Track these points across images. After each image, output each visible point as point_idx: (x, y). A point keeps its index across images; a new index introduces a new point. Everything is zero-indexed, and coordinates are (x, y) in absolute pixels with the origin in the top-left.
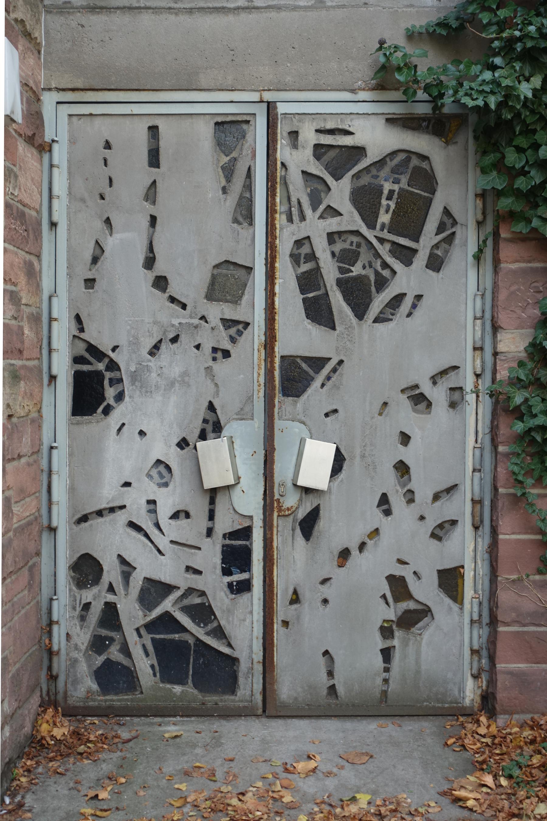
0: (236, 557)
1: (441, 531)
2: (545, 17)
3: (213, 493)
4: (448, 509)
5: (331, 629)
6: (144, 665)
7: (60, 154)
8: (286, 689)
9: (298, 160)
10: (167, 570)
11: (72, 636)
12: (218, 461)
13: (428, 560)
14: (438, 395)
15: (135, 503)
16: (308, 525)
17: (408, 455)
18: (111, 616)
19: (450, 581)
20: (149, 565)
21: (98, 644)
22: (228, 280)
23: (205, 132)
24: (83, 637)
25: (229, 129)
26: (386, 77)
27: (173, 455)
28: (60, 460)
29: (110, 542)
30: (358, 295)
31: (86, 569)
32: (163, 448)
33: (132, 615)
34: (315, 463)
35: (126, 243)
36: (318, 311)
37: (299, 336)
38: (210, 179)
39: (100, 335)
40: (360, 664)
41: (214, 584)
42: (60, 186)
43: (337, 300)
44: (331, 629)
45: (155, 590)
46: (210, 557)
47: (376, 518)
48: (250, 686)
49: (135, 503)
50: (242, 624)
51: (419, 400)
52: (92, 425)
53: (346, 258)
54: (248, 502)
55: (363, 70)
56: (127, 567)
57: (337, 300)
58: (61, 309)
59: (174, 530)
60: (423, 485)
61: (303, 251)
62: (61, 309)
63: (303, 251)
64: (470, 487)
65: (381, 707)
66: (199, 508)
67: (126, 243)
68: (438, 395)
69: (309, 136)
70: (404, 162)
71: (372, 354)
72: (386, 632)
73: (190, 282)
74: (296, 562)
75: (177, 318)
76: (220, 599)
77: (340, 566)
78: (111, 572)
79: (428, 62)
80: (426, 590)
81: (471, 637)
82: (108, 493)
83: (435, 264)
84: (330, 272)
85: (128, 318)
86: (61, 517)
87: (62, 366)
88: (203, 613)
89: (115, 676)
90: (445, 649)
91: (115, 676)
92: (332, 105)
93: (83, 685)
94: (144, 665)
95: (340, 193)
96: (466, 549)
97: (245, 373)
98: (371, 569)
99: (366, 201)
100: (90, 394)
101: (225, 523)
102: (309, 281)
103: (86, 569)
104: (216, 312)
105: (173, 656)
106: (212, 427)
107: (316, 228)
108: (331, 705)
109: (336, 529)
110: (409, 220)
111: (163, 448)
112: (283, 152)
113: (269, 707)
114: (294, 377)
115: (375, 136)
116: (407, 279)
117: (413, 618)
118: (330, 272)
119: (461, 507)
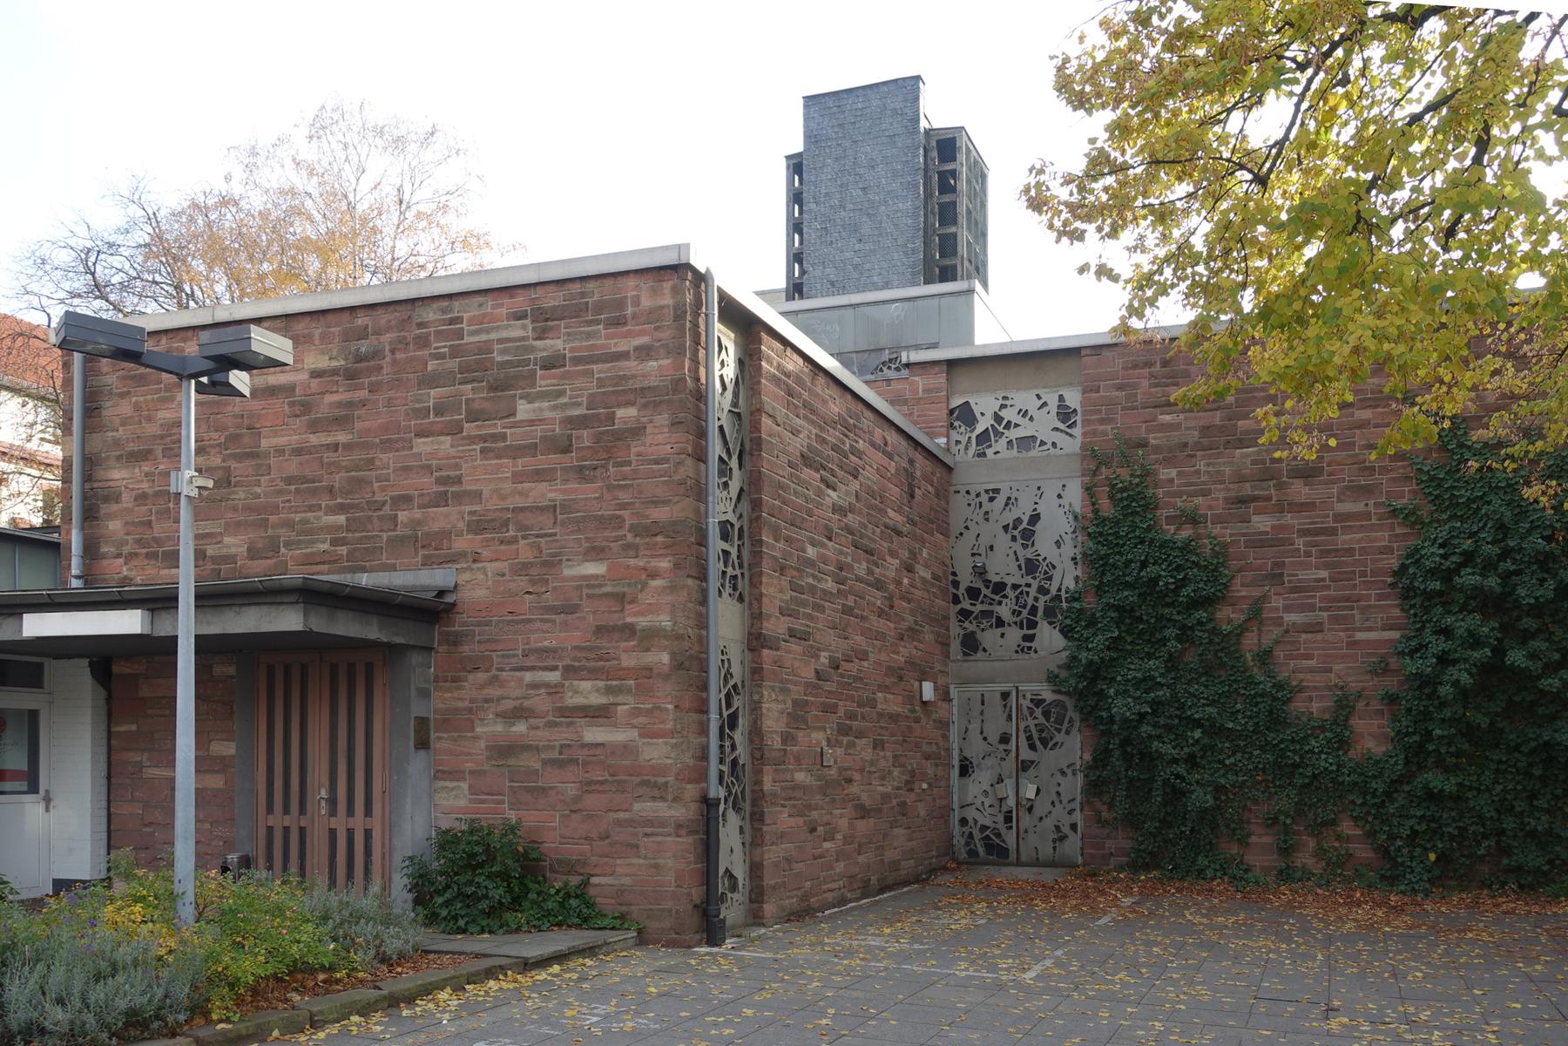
0: (1008, 819)
1: (1071, 812)
2: (1257, 8)
3: (1001, 800)
4: (1073, 805)
5: (1038, 842)
6: (981, 850)
7: (955, 702)
8: (1023, 858)
9: (1026, 703)
10: (987, 822)
11: (959, 841)
12: (1001, 791)
13: (1066, 821)
14: (1069, 772)
15: (978, 802)
16: (1030, 809)
17: (1060, 789)
18: (971, 835)
19: (1074, 827)
20: (982, 821)
21: (967, 844)
22: (1005, 739)
23: (998, 696)
24: (963, 842)
25: (1005, 695)
26: (1052, 679)
27: (989, 789)
28: (955, 790)
29: (971, 814)
30: (1044, 742)
31: (964, 822)
32: (986, 786)
33: (977, 835)
34: (1030, 793)
35: (974, 727)
36: (1032, 747)
37: (1026, 754)
38: (1000, 709)
39: (967, 754)
40: (1046, 850)
41: (1002, 827)
42: (955, 710)
43: (1038, 743)
44: (1038, 842)
45: (984, 828)
46: (1000, 818)
47: (1050, 807)
48: (1013, 857)
49: (978, 802)
50: (1010, 839)
51: (1063, 773)
52: (965, 780)
53: (1041, 731)
54: (1011, 802)
55: (1044, 676)
56: (976, 821)
57: (1038, 743)
58: (956, 746)
59: (989, 810)
60: (1065, 800)
61: (1027, 730)
62: (956, 746)
63: (1027, 730)
64: (1079, 799)
65: (1051, 864)
66: (997, 804)
67: (974, 727)
68: (1069, 772)
69: (1029, 696)
70: (1056, 703)
71: (1050, 759)
72: (1054, 841)
73: (994, 738)
74: (1026, 820)
75: (990, 749)
76: (1003, 831)
77: (1063, 84)
78: (971, 822)
79: (1064, 674)
80: (1066, 830)
81: (1079, 844)
82: (970, 799)
83: (1068, 733)
84: (1035, 735)
85: (975, 749)
86: (956, 806)
87: (956, 762)
88: (999, 835)
89: (973, 853)
90: (1072, 846)
91: (973, 853)
92: (1035, 687)
93: (963, 855)
94: (981, 850)
95: (1038, 712)
96: (1078, 817)
97: (1010, 765)
98: (1049, 823)
99: (1046, 714)
100: (965, 770)
101: (1004, 809)
102: (1029, 738)
103: (964, 822)
104: (1002, 747)
105: (990, 847)
106: (1000, 780)
107: (1031, 723)
108: (1037, 863)
109: (1039, 810)
110: (1060, 721)
111: (986, 786)
112: (1021, 701)
113: (1019, 863)
114: (1025, 766)
115: (1048, 696)
116: (1059, 737)
117: (1063, 838)
118: (1035, 735)
119: (1076, 805)
